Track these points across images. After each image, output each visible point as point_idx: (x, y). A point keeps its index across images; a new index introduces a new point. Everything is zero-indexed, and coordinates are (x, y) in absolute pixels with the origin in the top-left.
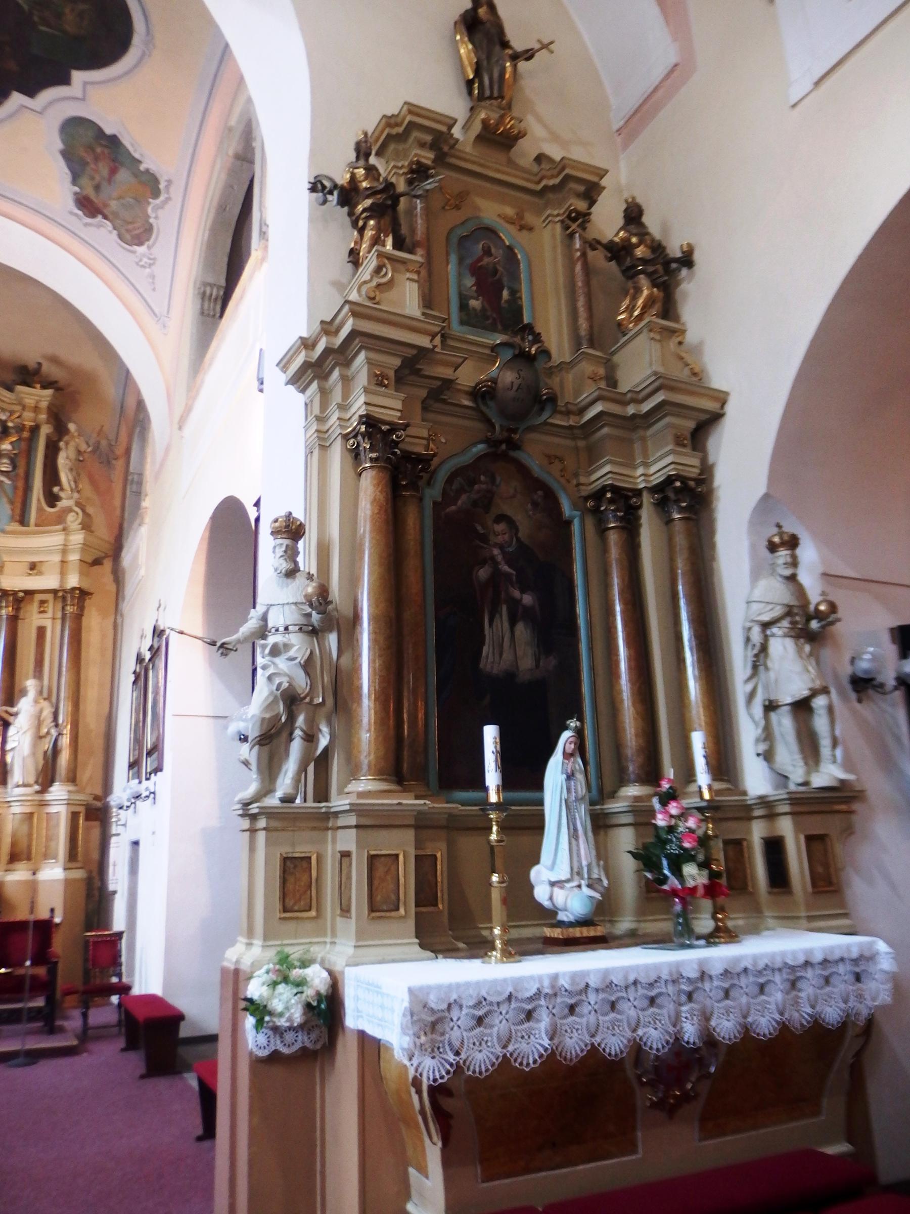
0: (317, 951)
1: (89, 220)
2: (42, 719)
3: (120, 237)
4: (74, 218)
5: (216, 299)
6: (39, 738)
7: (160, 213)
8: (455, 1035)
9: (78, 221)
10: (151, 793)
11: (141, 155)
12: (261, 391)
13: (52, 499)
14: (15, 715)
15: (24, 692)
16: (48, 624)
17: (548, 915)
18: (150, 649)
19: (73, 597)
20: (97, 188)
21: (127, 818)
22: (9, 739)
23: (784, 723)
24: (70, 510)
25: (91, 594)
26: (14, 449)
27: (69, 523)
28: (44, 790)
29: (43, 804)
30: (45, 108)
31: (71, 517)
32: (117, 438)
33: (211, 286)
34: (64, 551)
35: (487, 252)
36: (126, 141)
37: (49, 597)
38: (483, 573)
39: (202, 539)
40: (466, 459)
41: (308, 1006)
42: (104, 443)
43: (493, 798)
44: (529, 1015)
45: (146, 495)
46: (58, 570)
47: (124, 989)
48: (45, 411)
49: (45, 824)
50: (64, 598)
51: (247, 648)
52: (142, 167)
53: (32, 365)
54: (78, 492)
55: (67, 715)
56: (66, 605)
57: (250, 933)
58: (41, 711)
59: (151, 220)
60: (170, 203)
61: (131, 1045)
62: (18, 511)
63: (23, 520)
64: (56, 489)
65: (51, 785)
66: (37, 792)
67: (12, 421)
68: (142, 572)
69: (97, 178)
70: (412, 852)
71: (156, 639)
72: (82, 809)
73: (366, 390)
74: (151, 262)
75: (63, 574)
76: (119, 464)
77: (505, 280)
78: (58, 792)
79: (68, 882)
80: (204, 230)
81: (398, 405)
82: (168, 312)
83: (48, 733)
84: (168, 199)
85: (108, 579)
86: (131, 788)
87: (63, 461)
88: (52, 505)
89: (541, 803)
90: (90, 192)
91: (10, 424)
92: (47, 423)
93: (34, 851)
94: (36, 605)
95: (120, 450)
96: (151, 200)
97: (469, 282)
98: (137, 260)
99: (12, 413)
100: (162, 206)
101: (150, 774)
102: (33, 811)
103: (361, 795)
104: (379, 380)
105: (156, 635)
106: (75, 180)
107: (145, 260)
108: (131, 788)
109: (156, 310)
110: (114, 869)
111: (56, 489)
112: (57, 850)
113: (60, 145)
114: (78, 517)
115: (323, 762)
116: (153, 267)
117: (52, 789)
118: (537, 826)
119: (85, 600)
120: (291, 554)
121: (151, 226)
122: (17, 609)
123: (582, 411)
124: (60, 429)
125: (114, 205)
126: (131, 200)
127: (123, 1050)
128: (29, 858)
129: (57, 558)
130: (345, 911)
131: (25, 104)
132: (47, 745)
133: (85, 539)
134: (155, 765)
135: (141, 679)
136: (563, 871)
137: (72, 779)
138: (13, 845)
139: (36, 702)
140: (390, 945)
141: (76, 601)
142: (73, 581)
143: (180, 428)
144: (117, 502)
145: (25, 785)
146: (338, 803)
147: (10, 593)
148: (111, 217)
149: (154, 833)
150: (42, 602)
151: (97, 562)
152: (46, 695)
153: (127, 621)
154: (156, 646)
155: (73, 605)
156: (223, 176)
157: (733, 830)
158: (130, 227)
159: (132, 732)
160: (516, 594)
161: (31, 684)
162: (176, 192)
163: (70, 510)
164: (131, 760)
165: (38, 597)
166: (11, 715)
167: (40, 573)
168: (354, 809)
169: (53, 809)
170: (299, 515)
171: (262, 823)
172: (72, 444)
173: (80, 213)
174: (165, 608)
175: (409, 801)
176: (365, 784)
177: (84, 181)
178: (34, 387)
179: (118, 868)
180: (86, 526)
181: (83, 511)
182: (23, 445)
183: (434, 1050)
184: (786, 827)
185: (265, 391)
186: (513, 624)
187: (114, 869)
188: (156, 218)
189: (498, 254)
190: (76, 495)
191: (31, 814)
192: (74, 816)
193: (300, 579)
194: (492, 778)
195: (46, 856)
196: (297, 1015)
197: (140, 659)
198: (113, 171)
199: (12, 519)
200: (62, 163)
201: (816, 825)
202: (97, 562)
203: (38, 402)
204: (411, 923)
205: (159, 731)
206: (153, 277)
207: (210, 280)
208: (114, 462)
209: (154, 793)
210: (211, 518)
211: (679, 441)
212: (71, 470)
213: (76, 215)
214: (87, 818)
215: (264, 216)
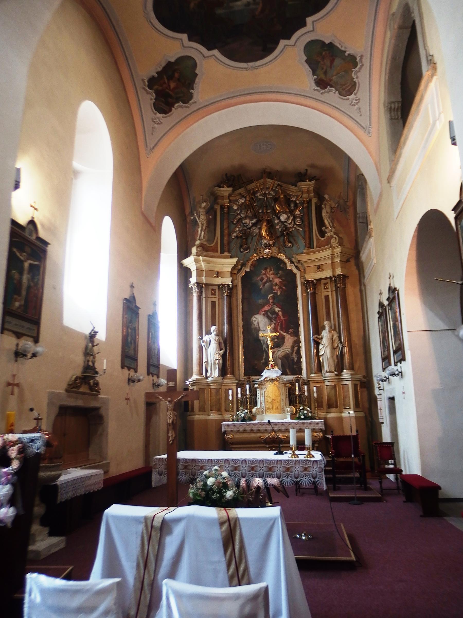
1: (323, 91)
2: (333, 340)
3: (340, 94)
4: (316, 92)
5: (398, 109)
6: (333, 349)
7: (359, 74)
10: (400, 372)
11: (345, 48)
12: (454, 144)
13: (322, 233)
14: (322, 339)
15: (324, 328)
16: (329, 294)
18: (388, 299)
19: (340, 279)
20: (325, 73)
21: (384, 386)
24: (332, 237)
25: (348, 277)
26: (301, 213)
27: (332, 243)
28: (340, 373)
29: (340, 380)
31: (333, 240)
32: (348, 198)
34: (332, 258)
37: (328, 281)
39: (413, 237)
42: (341, 201)
45: (371, 222)
46: (331, 267)
47: (397, 471)
48: (312, 192)
49: (342, 390)
50: (335, 281)
53: (303, 171)
54: (334, 227)
55: (345, 337)
56: (337, 284)
58: (333, 336)
60: (363, 67)
61: (409, 499)
62: (308, 242)
63: (311, 246)
64: (323, 228)
65: (342, 372)
66: (336, 375)
67: (298, 200)
68: (375, 261)
69: (325, 68)
71: (391, 294)
74: (357, 101)
75: (333, 269)
76: (351, 210)
78: (346, 374)
79: (356, 417)
80: (386, 74)
82: (370, 125)
83: (338, 346)
84: (362, 65)
85: (354, 268)
86: (389, 370)
87: (324, 214)
88: (323, 236)
90: (323, 76)
91: (298, 202)
92: (314, 197)
94: (322, 286)
95: (350, 203)
96: (353, 70)
98: (350, 103)
99: (297, 196)
100: (359, 71)
101: (397, 362)
102: (336, 384)
105: (391, 291)
106: (314, 74)
107: (354, 101)
108: (389, 370)
109: (364, 126)
110: (381, 412)
111: (323, 228)
113: (305, 58)
114: (336, 240)
116: (359, 104)
117: (343, 373)
119: (345, 280)
121: (355, 83)
122: (315, 289)
124: (321, 199)
126: (343, 73)
127: (404, 502)
128: (337, 407)
129: (329, 261)
131: (286, 44)
132: (338, 352)
133: (341, 250)
134: (401, 357)
135: (382, 315)
137: (352, 368)
138: (329, 399)
139: (330, 332)
141: (341, 281)
142: (339, 271)
143: (389, 182)
144: (353, 229)
145: (330, 372)
147: (310, 281)
148: (334, 85)
149: (404, 393)
150: (325, 284)
151: (348, 261)
152: (333, 328)
153: (368, 288)
154: (391, 297)
155: (340, 283)
156: (393, 41)
158: (344, 87)
159: (382, 343)
161: (326, 323)
162: (366, 61)
163: (332, 237)
164: (383, 357)
165: (323, 282)
166: (319, 339)
167: (323, 270)
169: (345, 383)
172: (328, 205)
173: (319, 88)
174: (393, 277)
177: (320, 72)
178: (306, 182)
179: (383, 411)
180: (341, 243)
181: (338, 236)
185: (458, 143)
187: (381, 412)
188: (357, 78)
190: (333, 229)
191: (335, 386)
192: (355, 386)
195: (345, 406)
197: (381, 305)
198: (332, 62)
199: (306, 246)
200: (307, 66)
202: (348, 261)
203: (308, 188)
205: (400, 340)
207: (393, 100)
208: (348, 210)
209: (401, 372)
210: (418, 225)
212: (329, 217)
213: (317, 90)
214: (361, 387)
215: (428, 51)
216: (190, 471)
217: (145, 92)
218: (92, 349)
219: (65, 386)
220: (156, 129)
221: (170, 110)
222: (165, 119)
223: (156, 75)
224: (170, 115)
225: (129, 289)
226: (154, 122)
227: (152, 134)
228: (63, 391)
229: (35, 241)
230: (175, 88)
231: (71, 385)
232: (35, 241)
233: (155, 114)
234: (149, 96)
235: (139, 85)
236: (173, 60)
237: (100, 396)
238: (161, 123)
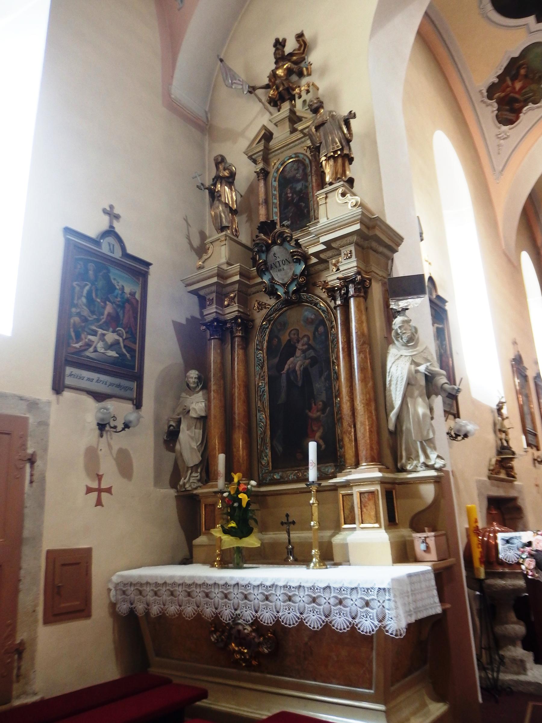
216: (297, 605)
217: (484, 105)
218: (502, 425)
219: (486, 472)
220: (503, 146)
221: (518, 118)
222: (513, 130)
223: (496, 80)
224: (519, 123)
225: (511, 346)
226: (499, 138)
227: (499, 153)
228: (485, 479)
229: (435, 300)
230: (522, 88)
231: (492, 470)
232: (435, 300)
233: (499, 128)
234: (490, 109)
235: (477, 98)
236: (516, 55)
237: (516, 483)
238: (508, 136)
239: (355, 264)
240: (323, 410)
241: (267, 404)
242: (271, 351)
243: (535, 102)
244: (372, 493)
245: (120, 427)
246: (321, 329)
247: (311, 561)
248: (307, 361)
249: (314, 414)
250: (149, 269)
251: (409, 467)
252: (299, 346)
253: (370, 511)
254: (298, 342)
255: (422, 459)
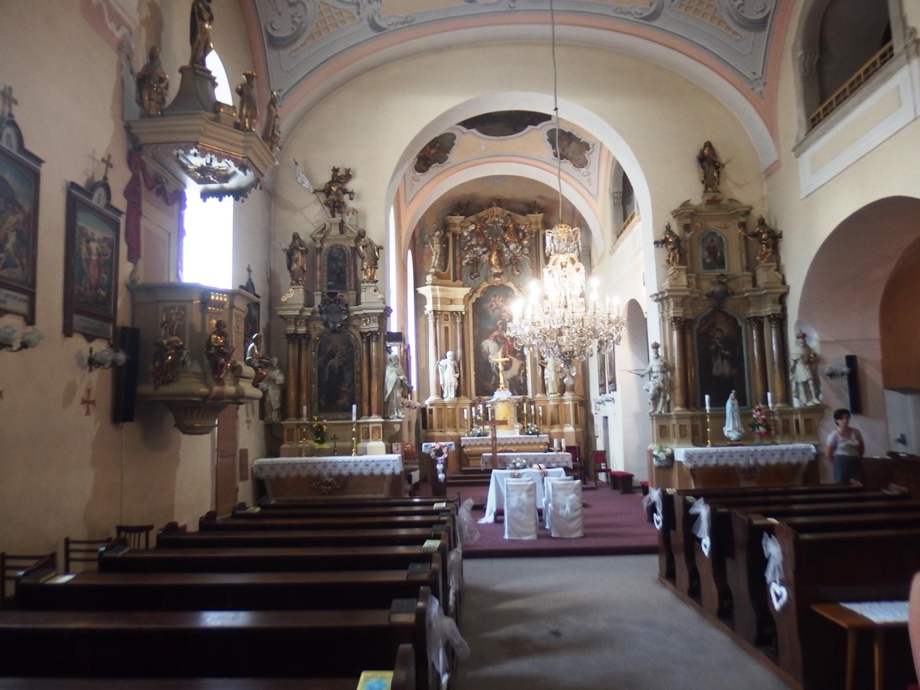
0: (669, 446)
3: (574, 165)
7: (591, 156)
8: (695, 459)
9: (556, 162)
17: (728, 439)
22: (545, 375)
23: (801, 388)
29: (562, 401)
30: (541, 128)
33: (616, 193)
35: (712, 241)
36: (574, 133)
38: (713, 347)
40: (706, 314)
41: (667, 456)
43: (708, 412)
44: (711, 457)
48: (540, 223)
51: (648, 375)
52: (582, 141)
57: (653, 442)
59: (587, 158)
65: (564, 393)
70: (690, 424)
72: (578, 402)
73: (673, 309)
77: (718, 249)
78: (568, 396)
79: (576, 433)
81: (682, 311)
84: (593, 151)
89: (725, 410)
91: (526, 231)
93: (560, 420)
97: (706, 253)
100: (591, 153)
103: (677, 411)
104: (676, 304)
112: (570, 419)
113: (547, 138)
115: (669, 403)
118: (724, 416)
120: (657, 353)
123: (743, 293)
125: (570, 154)
128: (559, 423)
130: (675, 437)
136: (731, 428)
138: (552, 418)
140: (371, 309)
145: (554, 393)
146: (672, 413)
157: (787, 417)
160: (723, 351)
168: (676, 415)
169: (567, 403)
170: (659, 342)
171: (654, 418)
175: (689, 413)
176: (678, 409)
182: (533, 241)
183: (690, 462)
184: (799, 417)
186: (722, 360)
188: (589, 157)
189: (716, 240)
192: (575, 406)
193: (660, 359)
194: (708, 408)
195: (566, 422)
196: (664, 458)
201: (808, 416)
204: (690, 440)
206: (589, 180)
211: (774, 302)
221: (428, 170)
230: (433, 154)
233: (415, 173)
239: (377, 326)
240: (349, 387)
241: (316, 380)
242: (320, 353)
243: (440, 163)
244: (378, 427)
245: (16, 345)
246: (350, 348)
247: (352, 453)
248: (342, 363)
249: (344, 389)
250: (40, 166)
251: (391, 417)
252: (337, 354)
253: (377, 434)
254: (337, 352)
255: (396, 414)
